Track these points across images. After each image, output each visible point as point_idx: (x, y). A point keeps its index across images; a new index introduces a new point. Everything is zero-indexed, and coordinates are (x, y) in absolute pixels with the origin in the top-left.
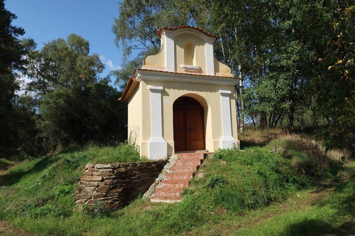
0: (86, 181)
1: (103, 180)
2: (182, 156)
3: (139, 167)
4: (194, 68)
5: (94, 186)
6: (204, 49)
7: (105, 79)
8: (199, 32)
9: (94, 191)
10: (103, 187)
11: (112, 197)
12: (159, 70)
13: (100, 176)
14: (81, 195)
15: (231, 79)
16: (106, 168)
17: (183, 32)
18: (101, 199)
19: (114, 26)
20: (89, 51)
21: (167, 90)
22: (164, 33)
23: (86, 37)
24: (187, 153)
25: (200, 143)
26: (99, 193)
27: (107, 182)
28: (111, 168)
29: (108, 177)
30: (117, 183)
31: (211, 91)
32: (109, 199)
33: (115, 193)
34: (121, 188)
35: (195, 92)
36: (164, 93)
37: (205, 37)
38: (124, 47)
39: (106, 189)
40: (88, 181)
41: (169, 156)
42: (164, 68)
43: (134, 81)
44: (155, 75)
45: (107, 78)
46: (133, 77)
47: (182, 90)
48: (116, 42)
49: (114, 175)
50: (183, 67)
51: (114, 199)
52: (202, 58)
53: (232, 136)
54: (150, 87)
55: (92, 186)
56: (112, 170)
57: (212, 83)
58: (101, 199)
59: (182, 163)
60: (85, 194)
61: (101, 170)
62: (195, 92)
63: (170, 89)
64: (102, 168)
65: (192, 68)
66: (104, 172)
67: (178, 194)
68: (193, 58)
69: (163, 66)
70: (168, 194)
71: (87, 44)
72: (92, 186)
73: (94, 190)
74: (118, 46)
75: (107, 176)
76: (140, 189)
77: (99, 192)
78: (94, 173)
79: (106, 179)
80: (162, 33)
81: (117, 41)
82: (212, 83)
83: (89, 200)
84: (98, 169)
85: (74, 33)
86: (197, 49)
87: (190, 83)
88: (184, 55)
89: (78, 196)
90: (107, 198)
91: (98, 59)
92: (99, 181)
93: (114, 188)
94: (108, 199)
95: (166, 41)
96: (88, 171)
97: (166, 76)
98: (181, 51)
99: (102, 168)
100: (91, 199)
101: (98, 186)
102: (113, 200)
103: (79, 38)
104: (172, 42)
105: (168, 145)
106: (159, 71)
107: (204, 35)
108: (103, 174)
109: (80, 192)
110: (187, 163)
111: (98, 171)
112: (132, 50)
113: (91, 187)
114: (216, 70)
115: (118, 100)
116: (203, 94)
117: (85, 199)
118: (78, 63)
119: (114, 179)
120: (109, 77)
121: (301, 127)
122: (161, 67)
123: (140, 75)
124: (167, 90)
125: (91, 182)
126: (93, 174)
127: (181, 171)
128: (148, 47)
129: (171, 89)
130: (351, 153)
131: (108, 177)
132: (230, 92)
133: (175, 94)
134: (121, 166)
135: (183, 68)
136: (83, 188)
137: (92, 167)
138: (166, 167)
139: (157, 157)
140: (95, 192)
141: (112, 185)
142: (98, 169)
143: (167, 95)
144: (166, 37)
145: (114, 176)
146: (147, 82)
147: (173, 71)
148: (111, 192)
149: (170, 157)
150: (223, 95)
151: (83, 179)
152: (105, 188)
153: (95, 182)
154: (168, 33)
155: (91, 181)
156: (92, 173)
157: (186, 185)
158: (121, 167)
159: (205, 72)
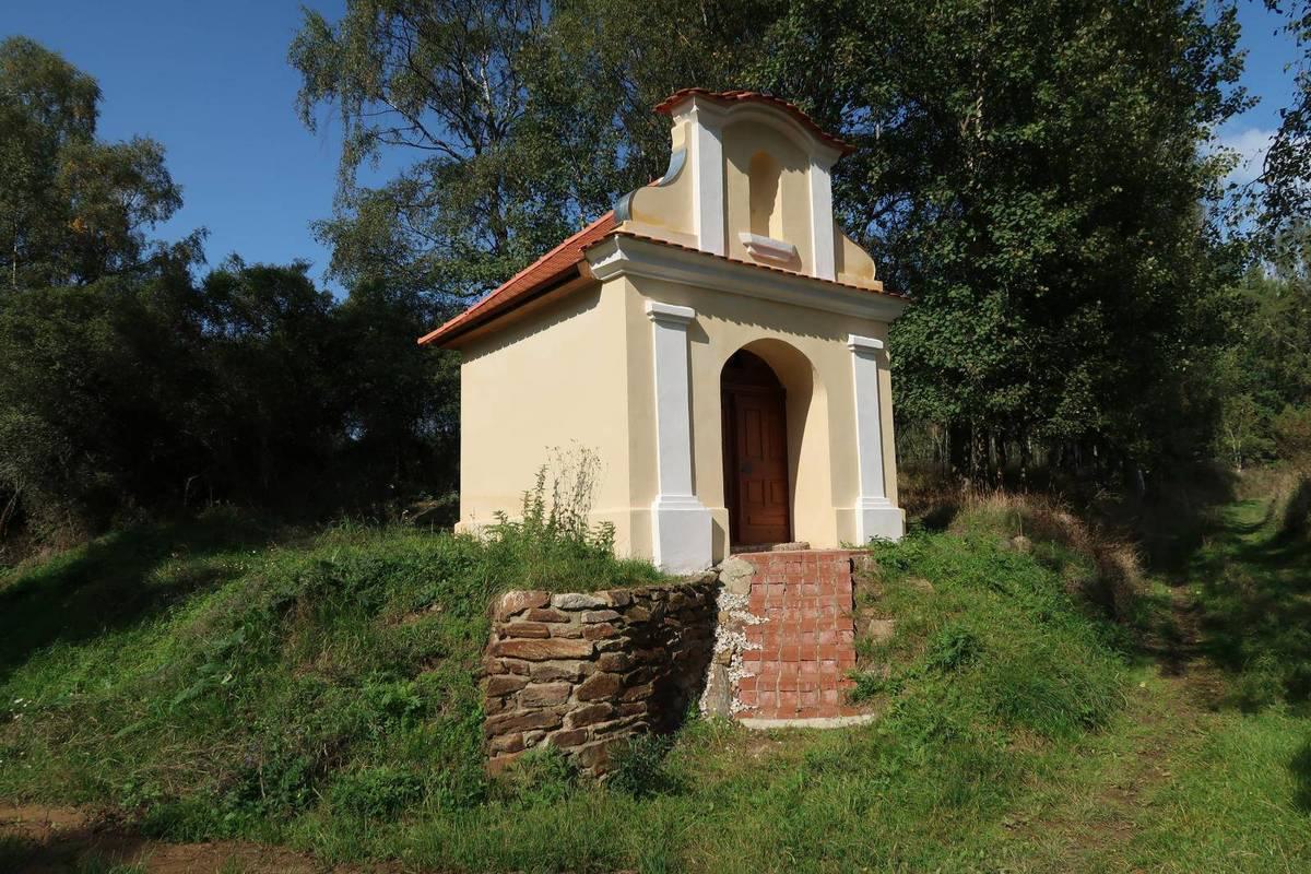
0: (527, 660)
1: (594, 656)
2: (764, 561)
3: (676, 601)
4: (782, 249)
5: (568, 679)
6: (804, 185)
7: (179, 247)
8: (796, 123)
9: (571, 699)
10: (600, 679)
11: (631, 717)
12: (670, 241)
13: (581, 637)
14: (508, 714)
15: (875, 297)
16: (598, 608)
17: (745, 115)
18: (602, 725)
19: (300, 42)
20: (93, 122)
21: (702, 320)
22: (695, 108)
23: (83, 62)
24: (749, 551)
25: (772, 518)
26: (590, 705)
27: (609, 660)
28: (610, 608)
29: (612, 642)
30: (639, 662)
31: (827, 335)
32: (626, 725)
33: (636, 700)
34: (651, 683)
35: (782, 336)
36: (695, 332)
37: (809, 142)
38: (347, 129)
39: (611, 687)
40: (534, 661)
41: (716, 562)
42: (693, 238)
43: (583, 272)
44: (672, 263)
45: (186, 243)
46: (580, 261)
47: (731, 320)
48: (302, 107)
49: (624, 634)
50: (751, 241)
51: (636, 724)
52: (796, 218)
53: (694, 494)
54: (649, 305)
55: (558, 678)
56: (614, 614)
57: (824, 307)
58: (602, 725)
59: (782, 587)
60: (530, 713)
61: (584, 616)
62: (782, 336)
63: (725, 321)
64: (584, 608)
65: (774, 247)
66: (594, 623)
67: (832, 696)
68: (770, 211)
69: (685, 232)
70: (795, 700)
71: (90, 94)
72: (558, 678)
73: (570, 694)
74: (312, 125)
75: (605, 638)
76: (686, 684)
77: (588, 700)
78: (553, 627)
79: (606, 649)
80: (687, 105)
81: (308, 103)
82: (824, 307)
83: (550, 735)
84: (567, 610)
85: (29, 36)
86: (785, 179)
87: (767, 300)
88: (748, 200)
89: (501, 722)
90: (617, 721)
91: (156, 160)
92: (583, 658)
93: (632, 683)
94: (622, 727)
95: (691, 136)
96: (529, 619)
97: (702, 268)
98: (741, 182)
99: (584, 608)
100: (561, 730)
101: (581, 677)
102: (634, 729)
103: (57, 62)
104: (716, 146)
105: (715, 525)
106: (687, 249)
107: (810, 137)
108: (593, 630)
109: (503, 703)
110: (799, 586)
111: (568, 621)
112: (382, 148)
113: (551, 681)
114: (839, 265)
115: (420, 341)
116: (803, 343)
117: (538, 729)
118: (64, 169)
119: (627, 648)
120: (196, 243)
121: (1020, 469)
122: (682, 234)
123: (625, 258)
124: (702, 320)
125: (548, 664)
126: (551, 630)
127: (791, 617)
128: (444, 145)
129: (714, 318)
130: (1149, 557)
131: (612, 642)
132: (878, 344)
133: (729, 336)
134: (636, 600)
135: (746, 245)
136: (515, 688)
137: (542, 605)
138: (723, 601)
139: (683, 567)
140: (573, 701)
141: (627, 672)
142: (567, 610)
143: (705, 339)
144: (696, 127)
145: (627, 638)
146: (643, 284)
147: (719, 251)
148: (625, 698)
149: (720, 567)
150: (861, 351)
151: (511, 653)
152: (608, 684)
153: (567, 662)
154: (709, 111)
155: (548, 659)
156: (547, 629)
157: (848, 664)
158: (635, 605)
159: (810, 268)
